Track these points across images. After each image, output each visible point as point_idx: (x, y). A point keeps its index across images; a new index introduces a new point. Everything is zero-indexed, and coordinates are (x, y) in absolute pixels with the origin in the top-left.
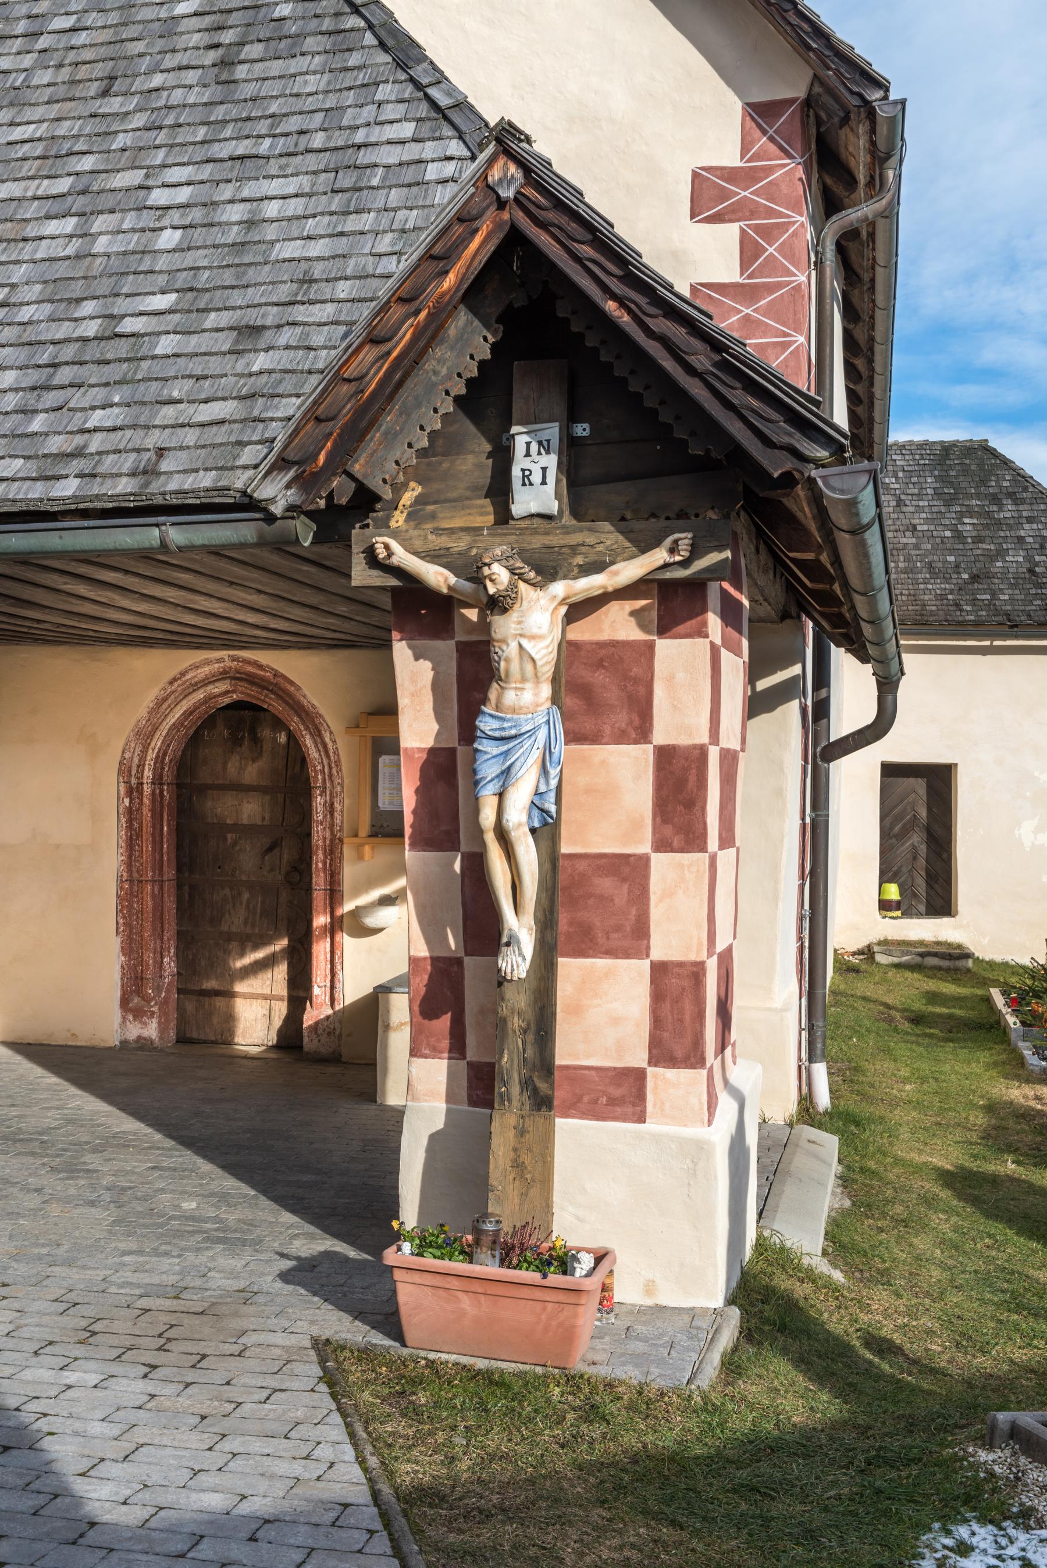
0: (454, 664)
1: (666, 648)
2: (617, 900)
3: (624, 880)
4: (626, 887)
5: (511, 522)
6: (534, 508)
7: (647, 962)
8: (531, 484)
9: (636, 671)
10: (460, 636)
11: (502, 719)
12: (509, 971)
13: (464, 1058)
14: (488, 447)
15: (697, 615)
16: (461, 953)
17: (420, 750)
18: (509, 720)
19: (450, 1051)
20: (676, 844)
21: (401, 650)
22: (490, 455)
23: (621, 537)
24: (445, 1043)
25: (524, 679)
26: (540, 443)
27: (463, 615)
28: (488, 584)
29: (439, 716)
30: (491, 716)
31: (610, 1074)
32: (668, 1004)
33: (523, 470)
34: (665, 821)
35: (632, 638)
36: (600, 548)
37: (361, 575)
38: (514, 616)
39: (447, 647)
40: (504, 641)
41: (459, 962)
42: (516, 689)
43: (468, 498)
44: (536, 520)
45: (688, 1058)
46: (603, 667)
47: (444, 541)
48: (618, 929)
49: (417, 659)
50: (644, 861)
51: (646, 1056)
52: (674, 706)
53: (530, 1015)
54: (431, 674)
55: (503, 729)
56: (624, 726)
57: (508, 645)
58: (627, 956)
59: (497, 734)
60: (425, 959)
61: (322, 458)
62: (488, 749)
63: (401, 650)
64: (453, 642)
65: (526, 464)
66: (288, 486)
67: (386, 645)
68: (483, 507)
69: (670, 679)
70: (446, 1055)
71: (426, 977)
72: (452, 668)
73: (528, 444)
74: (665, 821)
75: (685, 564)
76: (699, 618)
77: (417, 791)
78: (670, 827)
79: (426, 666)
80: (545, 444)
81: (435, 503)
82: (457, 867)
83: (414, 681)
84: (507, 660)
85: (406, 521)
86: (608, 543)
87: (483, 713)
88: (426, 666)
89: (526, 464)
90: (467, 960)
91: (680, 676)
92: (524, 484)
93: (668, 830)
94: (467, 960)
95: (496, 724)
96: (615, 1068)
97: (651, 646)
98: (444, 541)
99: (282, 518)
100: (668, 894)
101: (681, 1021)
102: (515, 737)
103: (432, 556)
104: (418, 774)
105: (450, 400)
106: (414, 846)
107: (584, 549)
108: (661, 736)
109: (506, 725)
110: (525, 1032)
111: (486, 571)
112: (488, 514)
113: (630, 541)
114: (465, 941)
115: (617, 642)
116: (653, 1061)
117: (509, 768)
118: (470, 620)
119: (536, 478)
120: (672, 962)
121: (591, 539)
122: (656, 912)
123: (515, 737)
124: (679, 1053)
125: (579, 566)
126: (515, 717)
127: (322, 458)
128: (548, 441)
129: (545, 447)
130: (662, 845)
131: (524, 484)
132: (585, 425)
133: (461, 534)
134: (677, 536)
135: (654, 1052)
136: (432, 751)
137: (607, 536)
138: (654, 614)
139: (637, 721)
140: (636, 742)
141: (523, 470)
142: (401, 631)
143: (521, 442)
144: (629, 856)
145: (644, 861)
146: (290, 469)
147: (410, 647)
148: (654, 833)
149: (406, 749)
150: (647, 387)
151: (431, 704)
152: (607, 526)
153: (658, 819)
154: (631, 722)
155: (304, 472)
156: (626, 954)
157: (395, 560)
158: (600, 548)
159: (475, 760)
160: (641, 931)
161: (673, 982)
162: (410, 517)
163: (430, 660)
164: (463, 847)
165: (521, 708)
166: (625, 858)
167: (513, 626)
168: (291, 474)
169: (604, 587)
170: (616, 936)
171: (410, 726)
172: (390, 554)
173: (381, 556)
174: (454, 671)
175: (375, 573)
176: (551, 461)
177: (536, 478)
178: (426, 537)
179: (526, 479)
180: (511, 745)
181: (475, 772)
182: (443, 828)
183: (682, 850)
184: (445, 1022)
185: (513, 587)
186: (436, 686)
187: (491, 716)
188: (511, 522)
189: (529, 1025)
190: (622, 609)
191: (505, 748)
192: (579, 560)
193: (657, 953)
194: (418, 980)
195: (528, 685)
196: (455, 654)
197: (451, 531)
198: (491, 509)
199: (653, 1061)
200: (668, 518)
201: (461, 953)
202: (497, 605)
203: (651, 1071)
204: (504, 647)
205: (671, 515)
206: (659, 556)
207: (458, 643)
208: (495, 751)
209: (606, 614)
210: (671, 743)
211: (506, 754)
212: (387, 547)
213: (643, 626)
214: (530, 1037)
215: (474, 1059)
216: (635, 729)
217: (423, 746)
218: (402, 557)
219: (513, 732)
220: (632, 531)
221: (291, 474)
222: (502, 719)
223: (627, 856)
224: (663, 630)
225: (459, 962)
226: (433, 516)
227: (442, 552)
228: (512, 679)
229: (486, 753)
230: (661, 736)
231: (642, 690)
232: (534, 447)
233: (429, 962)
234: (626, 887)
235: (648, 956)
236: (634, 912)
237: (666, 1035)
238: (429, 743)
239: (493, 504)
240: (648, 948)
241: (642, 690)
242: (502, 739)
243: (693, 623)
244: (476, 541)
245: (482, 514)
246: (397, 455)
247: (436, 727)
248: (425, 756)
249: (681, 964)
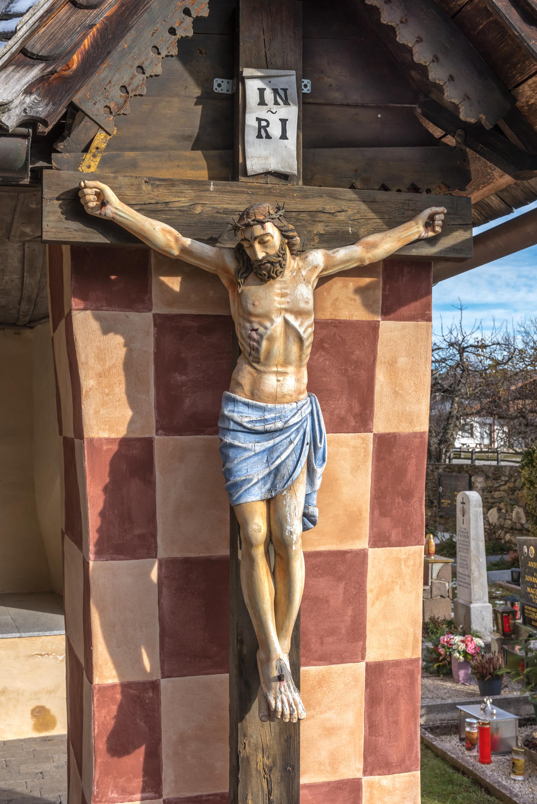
0: (151, 340)
1: (390, 330)
2: (332, 601)
3: (340, 579)
4: (342, 586)
5: (242, 179)
6: (274, 165)
7: (363, 665)
8: (268, 137)
9: (358, 354)
10: (159, 309)
11: (263, 409)
12: (287, 712)
13: (160, 796)
14: (197, 92)
15: (422, 297)
16: (157, 676)
17: (109, 441)
18: (271, 410)
19: (143, 791)
20: (393, 538)
21: (85, 324)
22: (199, 101)
23: (364, 207)
24: (138, 782)
25: (286, 363)
26: (275, 91)
27: (163, 284)
28: (257, 246)
29: (133, 400)
30: (247, 405)
31: (324, 790)
32: (383, 707)
33: (259, 120)
34: (383, 514)
35: (355, 318)
36: (342, 217)
37: (56, 225)
38: (277, 286)
39: (142, 321)
40: (267, 316)
41: (155, 686)
42: (277, 373)
43: (171, 148)
44: (270, 179)
45: (403, 761)
46: (324, 349)
47: (162, 194)
48: (332, 632)
49: (105, 331)
50: (361, 557)
51: (360, 765)
52: (396, 393)
53: (276, 750)
54: (122, 352)
55: (265, 421)
56: (343, 413)
57: (272, 321)
58: (342, 661)
59: (259, 427)
60: (113, 686)
61: (76, 58)
62: (249, 445)
63: (85, 324)
64: (148, 317)
65: (262, 113)
66: (28, 91)
67: (62, 317)
68: (194, 159)
69: (392, 364)
70: (139, 796)
71: (114, 708)
72: (148, 345)
73: (261, 91)
74: (383, 514)
75: (432, 241)
76: (424, 300)
77: (106, 489)
78: (388, 519)
79: (116, 341)
80: (282, 93)
81: (133, 149)
82: (154, 575)
83: (101, 359)
84: (271, 339)
85: (98, 167)
86: (350, 212)
87: (234, 401)
88: (116, 341)
89: (262, 113)
90: (164, 683)
91: (402, 361)
92: (259, 136)
93: (386, 523)
94: (164, 683)
95: (255, 415)
96: (329, 783)
97: (374, 327)
98: (162, 194)
99: (14, 135)
100: (385, 591)
101: (396, 723)
102: (281, 431)
103: (151, 211)
104: (107, 469)
105: (189, 21)
106: (100, 553)
107: (324, 217)
108: (381, 424)
109: (268, 416)
110: (270, 770)
111: (258, 230)
112: (202, 168)
113: (375, 211)
114: (162, 661)
115: (340, 322)
116: (368, 770)
117: (278, 468)
118: (171, 290)
119: (275, 130)
120: (388, 662)
121: (330, 207)
122: (373, 611)
123: (281, 431)
124: (394, 758)
125: (320, 235)
126: (278, 406)
127: (76, 58)
128: (285, 90)
129: (282, 96)
130: (379, 540)
131: (259, 136)
132: (219, 90)
133: (183, 187)
134: (435, 209)
135: (369, 759)
136: (124, 442)
137: (348, 205)
138: (379, 293)
139: (357, 409)
140: (355, 430)
141: (259, 120)
142: (84, 298)
143: (253, 87)
144: (345, 553)
145: (361, 557)
146: (33, 66)
147: (97, 318)
148: (372, 527)
149: (91, 440)
150: (419, 40)
151: (123, 387)
152: (350, 194)
153: (376, 512)
154: (350, 409)
155: (52, 73)
156: (341, 658)
157: (109, 211)
158: (342, 217)
159: (226, 459)
160: (357, 632)
161: (389, 683)
162: (104, 162)
163: (123, 334)
164: (161, 553)
165: (284, 396)
166: (340, 555)
167: (277, 299)
168: (35, 73)
169: (362, 260)
170: (331, 639)
171: (97, 412)
172: (104, 203)
173: (91, 204)
174: (151, 349)
175: (74, 225)
176: (291, 113)
177: (275, 130)
178: (139, 188)
179: (263, 132)
180: (278, 440)
181: (228, 473)
182: (137, 532)
183: (399, 544)
184: (138, 757)
185: (281, 254)
186: (129, 365)
187: (247, 405)
188: (242, 179)
189: (274, 762)
190: (346, 286)
191: (271, 443)
192: (320, 228)
193: (373, 655)
194: (104, 712)
195: (291, 369)
196: (152, 330)
197: (170, 183)
198: (204, 163)
199: (368, 770)
200: (399, 191)
201: (157, 676)
202: (264, 272)
203: (366, 780)
204: (268, 324)
205: (403, 189)
206: (416, 229)
207: (155, 315)
208: (259, 447)
209: (328, 291)
210: (392, 431)
211: (271, 450)
212: (100, 194)
213: (368, 306)
214: (276, 776)
215: (171, 796)
216: (355, 416)
217: (113, 436)
218: (118, 208)
219: (279, 425)
220: (374, 201)
221: (35, 73)
222: (263, 409)
223: (343, 554)
224: (387, 312)
225: (155, 686)
226: (134, 165)
227: (160, 207)
228: (274, 361)
229: (245, 449)
230: (381, 424)
231: (363, 374)
232: (269, 95)
233: (119, 689)
234: (342, 586)
235: (363, 658)
236: (350, 612)
237: (381, 739)
238: (121, 432)
239: (206, 157)
240: (364, 649)
241: (363, 374)
242: (265, 432)
243: (414, 306)
244: (201, 197)
245: (193, 168)
246: (125, 80)
247: (129, 413)
248: (115, 448)
249: (397, 664)
